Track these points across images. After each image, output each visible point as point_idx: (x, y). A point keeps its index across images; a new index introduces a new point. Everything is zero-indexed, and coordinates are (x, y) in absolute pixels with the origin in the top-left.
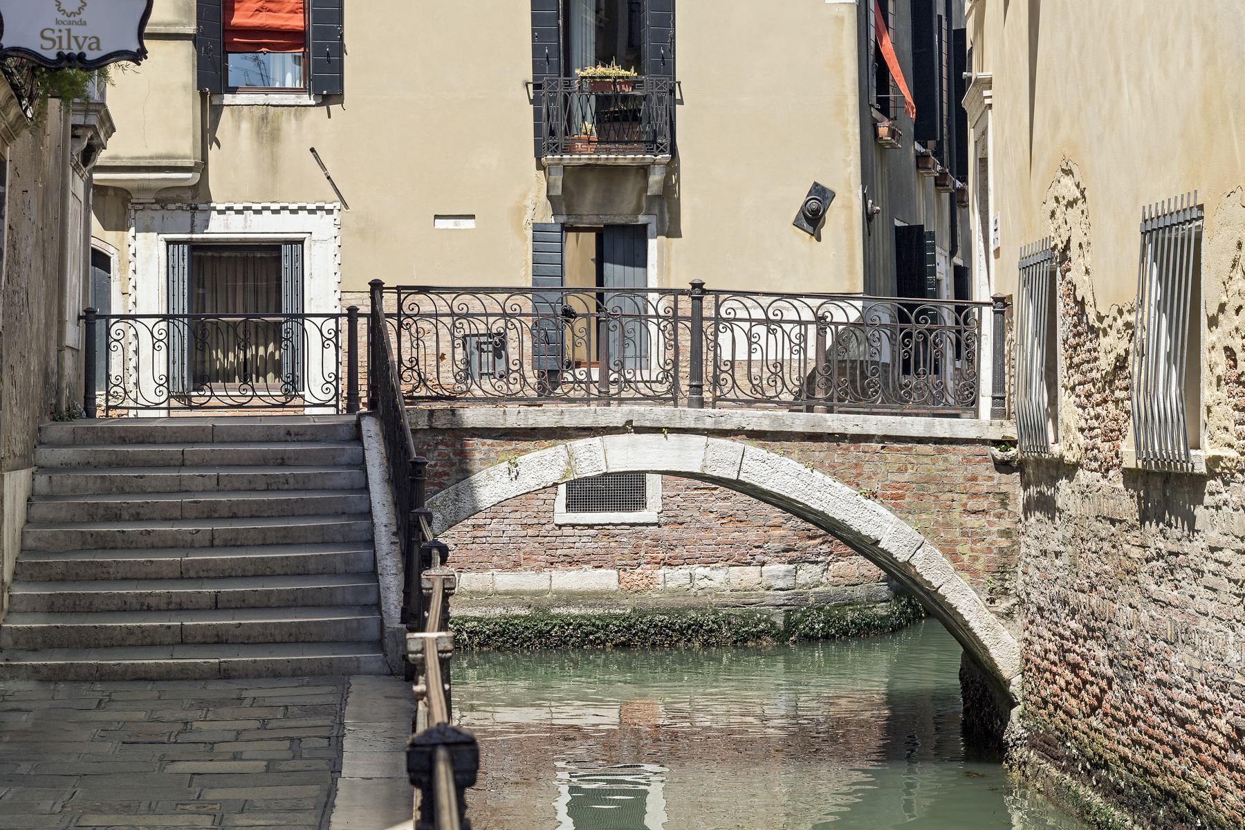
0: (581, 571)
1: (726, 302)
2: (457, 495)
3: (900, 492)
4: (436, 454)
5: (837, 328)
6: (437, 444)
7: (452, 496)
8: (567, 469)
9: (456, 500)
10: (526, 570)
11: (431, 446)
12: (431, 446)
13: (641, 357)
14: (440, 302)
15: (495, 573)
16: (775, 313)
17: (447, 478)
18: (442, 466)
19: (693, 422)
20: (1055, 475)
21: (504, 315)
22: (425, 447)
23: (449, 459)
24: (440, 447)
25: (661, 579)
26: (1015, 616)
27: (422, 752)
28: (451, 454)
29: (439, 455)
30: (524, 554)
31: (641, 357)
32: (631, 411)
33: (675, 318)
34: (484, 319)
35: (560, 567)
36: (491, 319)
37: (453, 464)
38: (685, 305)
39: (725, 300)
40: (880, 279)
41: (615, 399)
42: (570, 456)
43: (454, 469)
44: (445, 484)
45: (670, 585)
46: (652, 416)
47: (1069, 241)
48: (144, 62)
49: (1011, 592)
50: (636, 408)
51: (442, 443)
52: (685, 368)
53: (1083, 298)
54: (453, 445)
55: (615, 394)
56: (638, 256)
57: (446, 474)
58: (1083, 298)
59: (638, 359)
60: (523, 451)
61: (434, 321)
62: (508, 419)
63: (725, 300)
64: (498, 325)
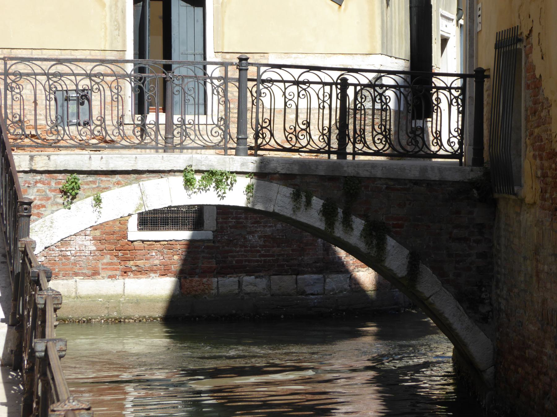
0: (149, 279)
1: (265, 73)
2: (52, 223)
3: (400, 222)
4: (35, 190)
5: (355, 89)
6: (36, 182)
7: (48, 224)
8: (140, 203)
9: (51, 227)
10: (103, 278)
11: (31, 184)
12: (31, 184)
13: (198, 104)
14: (35, 67)
15: (78, 280)
16: (291, 127)
17: (44, 209)
18: (40, 200)
19: (239, 167)
20: (519, 211)
21: (89, 76)
22: (27, 185)
23: (46, 194)
24: (39, 185)
25: (215, 285)
26: (489, 320)
27: (59, 415)
28: (47, 191)
29: (37, 192)
30: (102, 264)
31: (198, 104)
32: (190, 158)
33: (225, 79)
34: (73, 78)
35: (132, 275)
36: (79, 78)
37: (48, 199)
38: (233, 73)
39: (265, 71)
40: (395, 42)
41: (178, 148)
42: (142, 193)
43: (50, 202)
44: (42, 214)
45: (222, 290)
46: (207, 162)
47: (531, 31)
48: (102, 201)
49: (487, 301)
50: (195, 156)
51: (40, 181)
52: (234, 115)
53: (540, 76)
54: (49, 184)
55: (178, 145)
56: (197, 21)
57: (44, 206)
58: (540, 76)
59: (197, 106)
60: (104, 189)
61: (33, 81)
62: (93, 163)
63: (265, 71)
64: (84, 83)
